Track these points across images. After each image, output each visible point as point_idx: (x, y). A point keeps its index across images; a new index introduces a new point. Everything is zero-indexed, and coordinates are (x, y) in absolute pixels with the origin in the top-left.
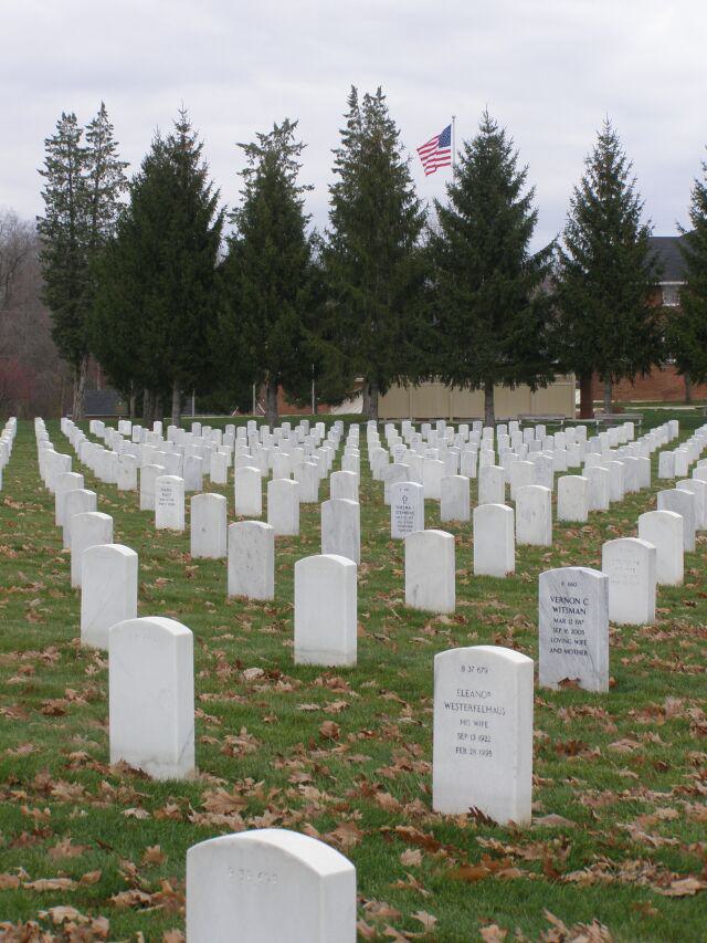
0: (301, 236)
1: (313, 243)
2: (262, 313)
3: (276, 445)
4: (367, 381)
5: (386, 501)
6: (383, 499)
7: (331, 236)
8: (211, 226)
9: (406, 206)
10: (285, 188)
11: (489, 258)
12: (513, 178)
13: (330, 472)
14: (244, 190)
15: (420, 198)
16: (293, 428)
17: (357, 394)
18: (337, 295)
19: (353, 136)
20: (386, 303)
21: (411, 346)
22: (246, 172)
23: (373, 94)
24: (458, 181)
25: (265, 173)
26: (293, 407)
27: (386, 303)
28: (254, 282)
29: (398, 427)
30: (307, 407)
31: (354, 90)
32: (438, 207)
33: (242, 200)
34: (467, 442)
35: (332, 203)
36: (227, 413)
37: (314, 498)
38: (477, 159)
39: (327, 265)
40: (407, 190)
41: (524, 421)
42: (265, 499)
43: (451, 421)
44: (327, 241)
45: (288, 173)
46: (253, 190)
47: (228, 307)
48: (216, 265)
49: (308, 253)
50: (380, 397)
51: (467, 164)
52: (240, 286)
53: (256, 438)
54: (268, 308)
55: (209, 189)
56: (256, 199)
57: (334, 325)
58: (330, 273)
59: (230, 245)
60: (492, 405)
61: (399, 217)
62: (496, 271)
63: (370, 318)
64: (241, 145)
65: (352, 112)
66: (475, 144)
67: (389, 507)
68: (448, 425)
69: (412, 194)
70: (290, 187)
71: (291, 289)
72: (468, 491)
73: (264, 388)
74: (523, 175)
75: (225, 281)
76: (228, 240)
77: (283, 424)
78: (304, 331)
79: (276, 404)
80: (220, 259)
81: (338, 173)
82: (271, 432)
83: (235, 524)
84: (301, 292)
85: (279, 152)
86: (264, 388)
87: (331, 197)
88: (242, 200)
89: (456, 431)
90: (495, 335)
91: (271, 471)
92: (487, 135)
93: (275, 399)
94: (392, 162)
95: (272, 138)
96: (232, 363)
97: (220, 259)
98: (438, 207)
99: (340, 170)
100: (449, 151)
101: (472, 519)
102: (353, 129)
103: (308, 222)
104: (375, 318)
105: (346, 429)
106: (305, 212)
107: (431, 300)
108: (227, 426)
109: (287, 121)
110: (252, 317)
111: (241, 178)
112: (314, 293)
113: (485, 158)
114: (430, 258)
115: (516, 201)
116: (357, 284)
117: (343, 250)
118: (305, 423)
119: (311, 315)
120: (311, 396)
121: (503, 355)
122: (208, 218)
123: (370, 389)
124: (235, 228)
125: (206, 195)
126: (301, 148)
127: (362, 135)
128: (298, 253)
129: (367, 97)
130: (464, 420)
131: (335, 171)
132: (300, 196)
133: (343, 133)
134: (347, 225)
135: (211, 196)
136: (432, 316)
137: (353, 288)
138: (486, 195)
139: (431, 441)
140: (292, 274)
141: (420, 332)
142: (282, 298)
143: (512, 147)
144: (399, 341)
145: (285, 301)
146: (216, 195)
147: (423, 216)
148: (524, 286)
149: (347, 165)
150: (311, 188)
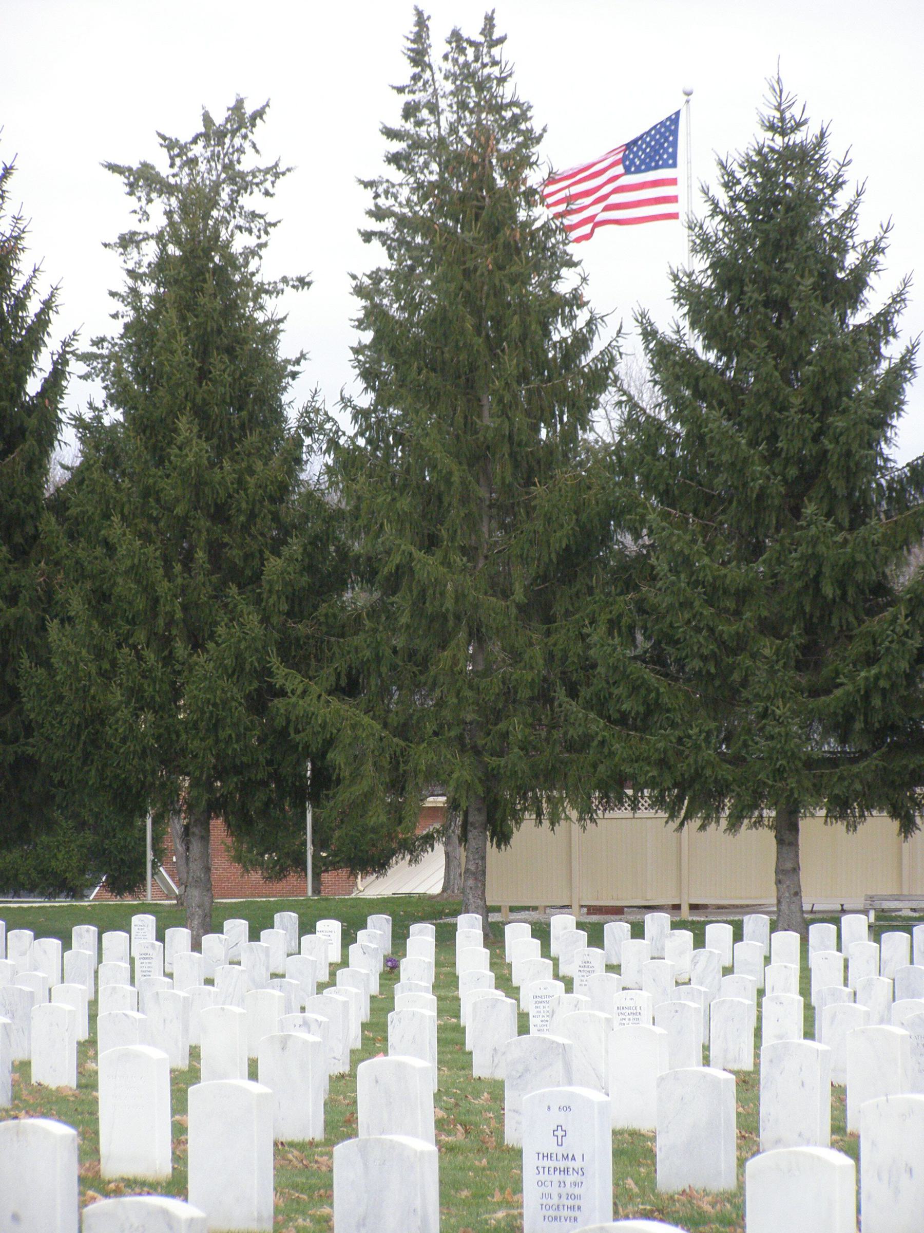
0: (277, 415)
1: (309, 432)
2: (170, 623)
3: (209, 982)
4: (454, 805)
5: (510, 1138)
6: (499, 1132)
7: (360, 414)
8: (33, 386)
9: (560, 332)
10: (231, 283)
11: (793, 472)
12: (852, 259)
13: (356, 1058)
14: (123, 290)
15: (599, 311)
16: (254, 936)
17: (428, 840)
18: (375, 573)
19: (417, 144)
20: (506, 594)
21: (574, 707)
22: (128, 241)
23: (473, 31)
24: (700, 265)
25: (178, 243)
26: (256, 876)
27: (506, 594)
28: (146, 537)
29: (542, 932)
30: (292, 879)
31: (422, 22)
32: (649, 333)
33: (115, 316)
34: (728, 971)
35: (361, 325)
36: (76, 892)
37: (316, 1132)
38: (752, 203)
39: (347, 492)
40: (563, 287)
41: (882, 915)
42: (179, 1132)
43: (685, 914)
44: (347, 425)
45: (240, 243)
46: (148, 289)
47: (77, 606)
48: (49, 491)
49: (296, 462)
50: (491, 851)
51: (727, 218)
52: (110, 549)
53: (157, 964)
54: (185, 608)
55: (27, 287)
56: (153, 316)
57: (367, 654)
58: (356, 514)
59: (82, 440)
60: (796, 870)
61: (541, 363)
62: (810, 509)
63: (462, 635)
64: (114, 168)
65: (416, 78)
66: (749, 165)
67: (518, 1153)
68: (675, 926)
69: (576, 300)
70: (247, 282)
71: (247, 557)
72: (731, 1106)
73: (176, 825)
74: (877, 249)
75: (71, 536)
76: (79, 422)
77: (228, 924)
78: (282, 675)
79: (208, 870)
80: (57, 475)
81: (376, 242)
82: (196, 946)
83: (103, 1204)
84: (274, 564)
85: (216, 187)
86: (176, 825)
87: (357, 307)
88: (115, 316)
89: (699, 942)
90: (804, 680)
91: (194, 1053)
92: (779, 140)
93: (206, 856)
94: (522, 215)
95: (198, 150)
96: (87, 758)
97: (57, 475)
98: (649, 333)
99: (381, 235)
100: (673, 182)
101: (741, 1186)
102: (419, 123)
103: (294, 375)
104: (477, 635)
105: (400, 937)
106: (285, 349)
107: (629, 586)
108: (77, 930)
109: (240, 104)
110: (141, 636)
111: (114, 255)
112: (311, 569)
113: (777, 202)
114: (626, 473)
115: (859, 318)
116: (431, 543)
117: (389, 452)
118: (287, 920)
119: (302, 629)
120: (304, 843)
121: (826, 734)
122: (25, 367)
123: (465, 826)
124: (96, 391)
125: (20, 304)
126: (277, 175)
127: (441, 142)
128: (267, 459)
129: (456, 37)
130: (722, 911)
131: (367, 237)
132: (272, 307)
133: (391, 134)
134: (402, 382)
135: (33, 307)
136: (631, 629)
137: (419, 554)
138: (782, 306)
139: (629, 974)
140: (252, 516)
141: (601, 670)
142: (224, 583)
143: (848, 174)
144: (544, 696)
145: (233, 590)
146: (48, 305)
147: (608, 360)
148: (883, 549)
149: (402, 222)
150: (303, 283)
